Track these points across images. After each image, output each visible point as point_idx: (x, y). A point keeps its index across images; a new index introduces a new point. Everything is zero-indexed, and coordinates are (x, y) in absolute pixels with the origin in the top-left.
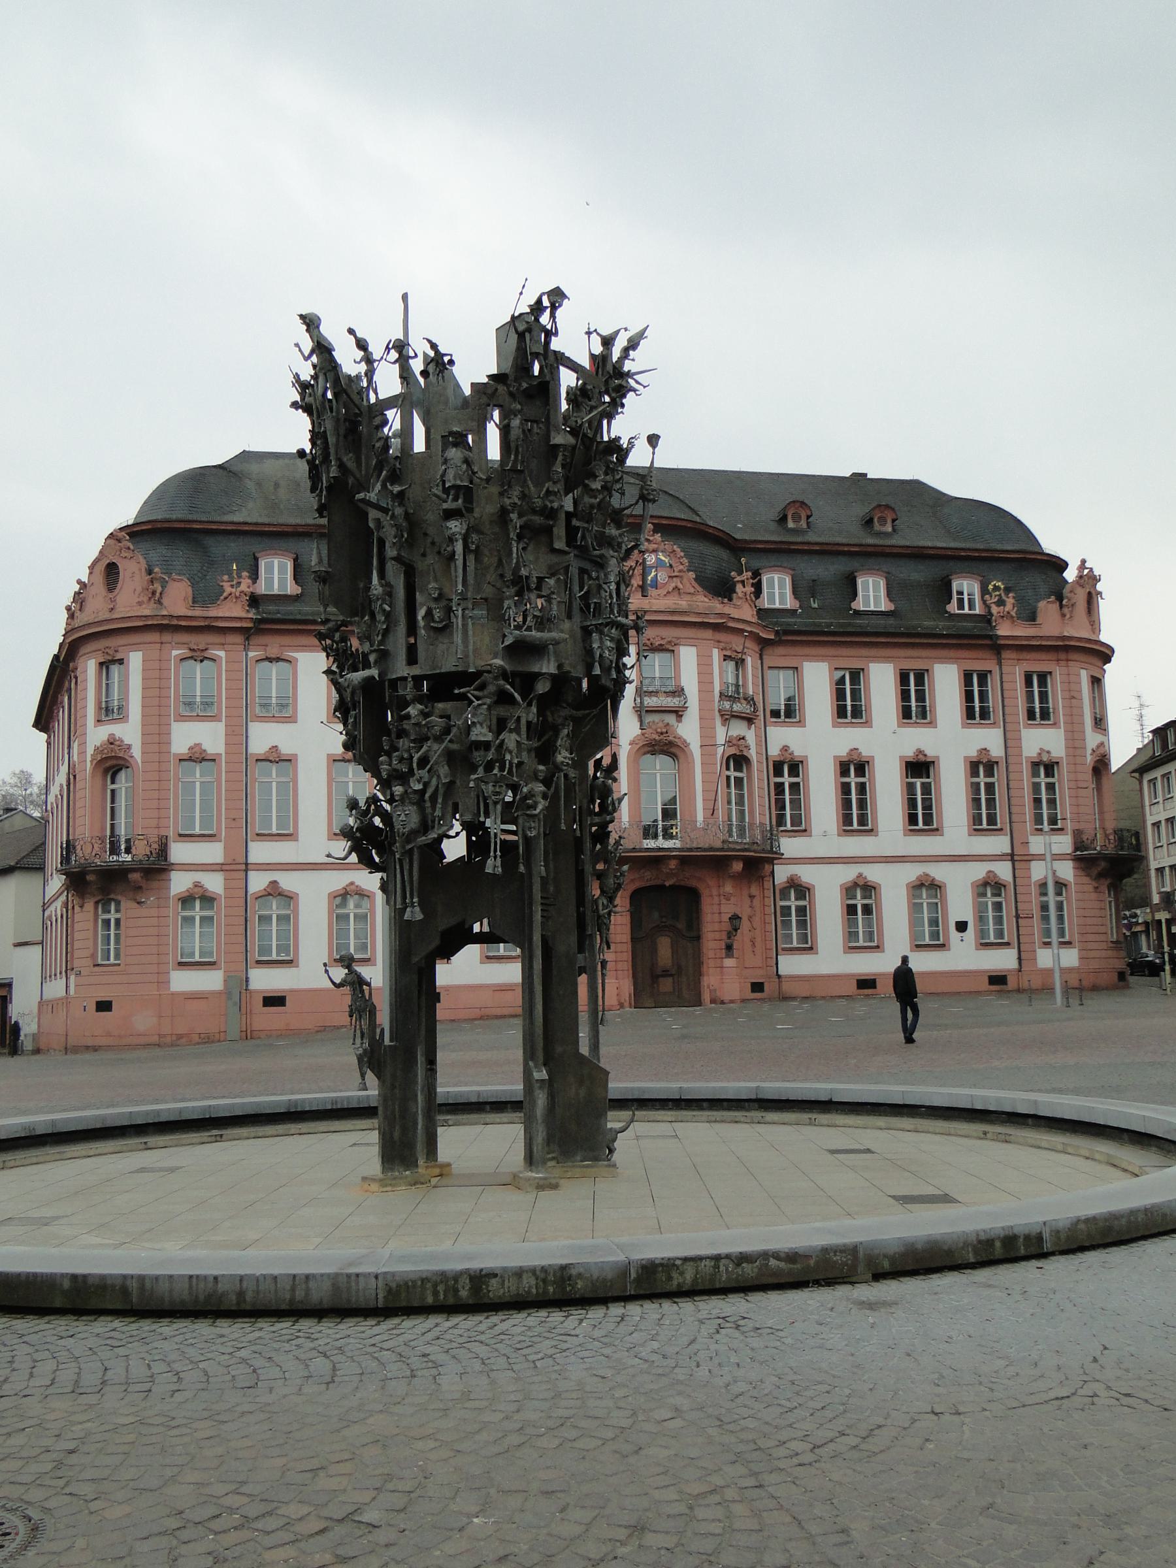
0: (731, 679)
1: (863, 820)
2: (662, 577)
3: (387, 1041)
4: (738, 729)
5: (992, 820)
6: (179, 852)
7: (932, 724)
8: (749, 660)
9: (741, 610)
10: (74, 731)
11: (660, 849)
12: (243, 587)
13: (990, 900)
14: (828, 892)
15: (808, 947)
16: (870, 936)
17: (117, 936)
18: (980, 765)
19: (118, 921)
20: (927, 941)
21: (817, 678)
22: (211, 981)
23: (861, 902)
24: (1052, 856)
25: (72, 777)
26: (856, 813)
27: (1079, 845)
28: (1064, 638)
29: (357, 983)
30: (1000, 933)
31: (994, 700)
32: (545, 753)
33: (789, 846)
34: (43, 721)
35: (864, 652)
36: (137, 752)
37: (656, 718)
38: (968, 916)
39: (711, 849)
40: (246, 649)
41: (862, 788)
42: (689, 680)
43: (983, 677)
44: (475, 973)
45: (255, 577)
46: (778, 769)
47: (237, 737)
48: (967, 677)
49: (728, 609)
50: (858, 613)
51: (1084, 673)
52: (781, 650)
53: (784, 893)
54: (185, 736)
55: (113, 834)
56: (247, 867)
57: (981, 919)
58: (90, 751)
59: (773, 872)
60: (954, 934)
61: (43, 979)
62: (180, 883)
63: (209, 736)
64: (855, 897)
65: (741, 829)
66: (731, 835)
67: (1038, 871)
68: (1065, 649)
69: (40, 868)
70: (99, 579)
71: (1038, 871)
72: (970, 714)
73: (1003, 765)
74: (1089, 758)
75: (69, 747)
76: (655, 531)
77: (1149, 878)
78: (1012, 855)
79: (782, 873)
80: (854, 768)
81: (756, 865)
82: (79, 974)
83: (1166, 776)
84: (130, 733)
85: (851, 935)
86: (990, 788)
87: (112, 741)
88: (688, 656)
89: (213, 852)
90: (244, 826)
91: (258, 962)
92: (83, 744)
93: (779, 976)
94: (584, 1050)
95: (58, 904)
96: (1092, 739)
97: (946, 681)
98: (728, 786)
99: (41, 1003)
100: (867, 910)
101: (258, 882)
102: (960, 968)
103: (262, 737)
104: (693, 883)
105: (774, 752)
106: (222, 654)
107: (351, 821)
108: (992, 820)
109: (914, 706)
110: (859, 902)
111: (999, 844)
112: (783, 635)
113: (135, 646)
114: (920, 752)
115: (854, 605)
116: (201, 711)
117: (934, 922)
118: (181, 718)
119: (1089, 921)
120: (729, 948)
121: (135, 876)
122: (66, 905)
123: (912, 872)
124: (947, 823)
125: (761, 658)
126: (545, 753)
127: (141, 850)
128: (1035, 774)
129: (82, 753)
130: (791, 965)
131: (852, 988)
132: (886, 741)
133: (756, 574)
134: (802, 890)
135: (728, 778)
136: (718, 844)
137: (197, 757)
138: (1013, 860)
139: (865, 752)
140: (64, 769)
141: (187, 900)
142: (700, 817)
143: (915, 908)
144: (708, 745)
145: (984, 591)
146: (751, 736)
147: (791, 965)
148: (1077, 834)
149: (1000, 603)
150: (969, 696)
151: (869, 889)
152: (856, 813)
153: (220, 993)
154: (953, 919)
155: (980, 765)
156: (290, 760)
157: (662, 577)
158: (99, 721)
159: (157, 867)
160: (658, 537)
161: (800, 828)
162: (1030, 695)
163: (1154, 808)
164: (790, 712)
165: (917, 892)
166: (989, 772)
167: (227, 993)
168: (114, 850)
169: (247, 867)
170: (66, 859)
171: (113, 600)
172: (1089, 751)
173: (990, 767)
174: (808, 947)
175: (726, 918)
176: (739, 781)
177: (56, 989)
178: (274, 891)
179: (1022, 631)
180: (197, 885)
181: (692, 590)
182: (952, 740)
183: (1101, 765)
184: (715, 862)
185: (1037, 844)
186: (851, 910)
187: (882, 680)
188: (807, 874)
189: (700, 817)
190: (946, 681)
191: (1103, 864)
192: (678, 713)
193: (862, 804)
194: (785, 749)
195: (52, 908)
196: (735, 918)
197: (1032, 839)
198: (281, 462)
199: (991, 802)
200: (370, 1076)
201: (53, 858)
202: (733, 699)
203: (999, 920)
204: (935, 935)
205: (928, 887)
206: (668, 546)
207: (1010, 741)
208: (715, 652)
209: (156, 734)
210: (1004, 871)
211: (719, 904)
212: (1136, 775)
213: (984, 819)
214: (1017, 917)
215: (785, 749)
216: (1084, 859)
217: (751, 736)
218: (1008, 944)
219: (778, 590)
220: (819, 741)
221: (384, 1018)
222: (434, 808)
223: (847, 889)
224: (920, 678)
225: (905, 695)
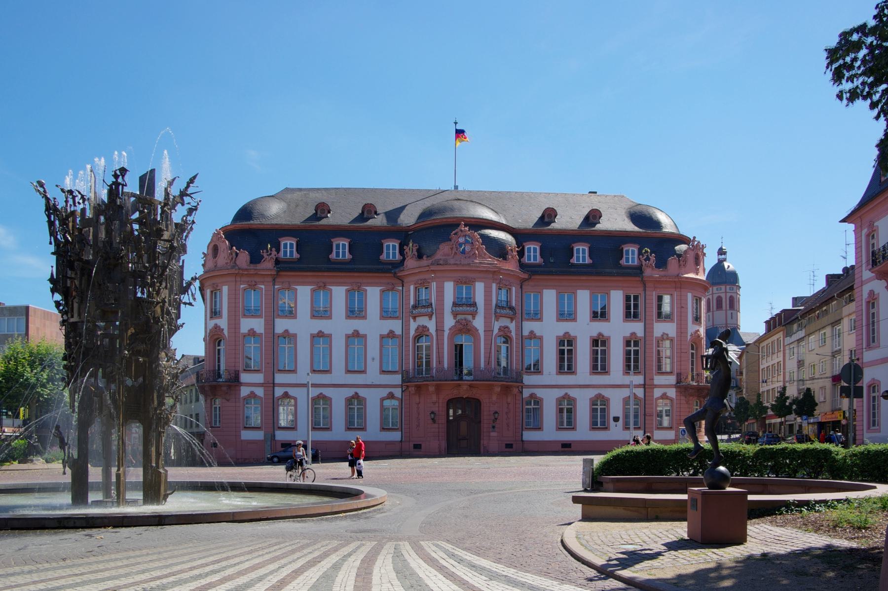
0: (504, 298)
1: (569, 368)
4: (505, 322)
5: (636, 367)
6: (245, 377)
7: (608, 320)
12: (273, 255)
14: (549, 400)
15: (539, 428)
22: (259, 435)
36: (226, 332)
37: (462, 317)
38: (620, 414)
40: (274, 285)
42: (479, 297)
45: (278, 251)
47: (270, 325)
50: (573, 265)
54: (247, 324)
56: (644, 386)
57: (626, 416)
60: (612, 423)
62: (244, 391)
63: (257, 324)
67: (657, 393)
70: (211, 252)
71: (657, 393)
74: (689, 337)
76: (466, 225)
78: (644, 385)
79: (526, 393)
80: (599, 342)
84: (223, 323)
86: (636, 352)
87: (216, 327)
89: (259, 378)
90: (272, 367)
93: (522, 441)
101: (279, 392)
103: (281, 325)
106: (263, 287)
108: (636, 367)
110: (565, 406)
111: (639, 379)
113: (224, 283)
115: (571, 261)
116: (254, 314)
118: (245, 316)
124: (579, 370)
125: (521, 287)
131: (559, 448)
132: (584, 330)
134: (538, 402)
137: (252, 333)
138: (644, 388)
144: (488, 330)
145: (640, 253)
149: (648, 259)
151: (327, 400)
154: (612, 415)
156: (330, 336)
158: (211, 317)
159: (235, 381)
160: (467, 229)
164: (291, 314)
166: (636, 344)
169: (274, 385)
171: (216, 262)
172: (689, 334)
178: (532, 396)
180: (566, 394)
182: (618, 329)
185: (658, 380)
188: (540, 393)
190: (617, 300)
192: (474, 314)
193: (570, 360)
197: (656, 377)
198: (303, 193)
200: (68, 471)
202: (503, 308)
204: (603, 423)
207: (648, 329)
209: (234, 325)
214: (645, 415)
217: (512, 326)
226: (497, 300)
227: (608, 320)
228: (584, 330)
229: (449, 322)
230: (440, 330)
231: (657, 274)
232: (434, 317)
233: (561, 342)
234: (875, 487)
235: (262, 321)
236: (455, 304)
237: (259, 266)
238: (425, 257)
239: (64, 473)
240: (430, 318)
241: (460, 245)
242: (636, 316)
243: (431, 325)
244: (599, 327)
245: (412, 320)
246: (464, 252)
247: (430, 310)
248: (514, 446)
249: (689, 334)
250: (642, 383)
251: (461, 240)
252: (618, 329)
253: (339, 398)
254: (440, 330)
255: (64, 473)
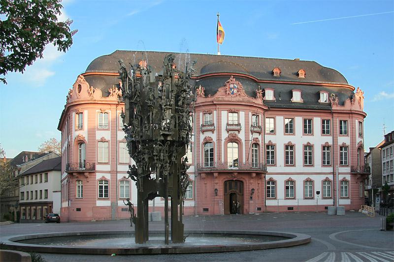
1: (292, 162)
2: (235, 91)
3: (137, 217)
4: (256, 135)
5: (328, 163)
7: (313, 135)
8: (260, 115)
9: (259, 101)
10: (69, 132)
11: (232, 170)
13: (327, 186)
14: (281, 182)
16: (292, 195)
17: (82, 190)
18: (325, 147)
19: (82, 186)
20: (308, 197)
21: (281, 121)
23: (290, 186)
24: (344, 172)
25: (69, 146)
26: (289, 160)
27: (352, 170)
28: (351, 111)
29: (130, 204)
30: (346, 195)
31: (331, 129)
32: (170, 157)
33: (270, 169)
34: (60, 128)
35: (293, 113)
36: (86, 139)
37: (232, 132)
39: (247, 170)
41: (292, 153)
43: (328, 121)
44: (158, 203)
46: (268, 147)
48: (323, 122)
49: (254, 100)
51: (357, 121)
52: (269, 112)
53: (268, 183)
55: (80, 162)
56: (117, 172)
58: (74, 138)
59: (265, 177)
61: (62, 202)
62: (99, 176)
64: (288, 184)
65: (256, 165)
66: (253, 166)
67: (341, 177)
68: (351, 113)
69: (60, 170)
72: (323, 132)
73: (332, 147)
75: (68, 136)
77: (382, 179)
78: (333, 173)
79: (268, 177)
80: (290, 147)
81: (260, 174)
82: (71, 201)
83: (391, 148)
85: (287, 195)
86: (328, 154)
88: (242, 114)
89: (108, 168)
91: (120, 199)
92: (71, 136)
94: (179, 220)
95: (66, 181)
96: (358, 140)
97: (317, 122)
98: (253, 152)
99: (61, 208)
100: (292, 187)
102: (273, 205)
104: (241, 180)
105: (267, 142)
107: (130, 170)
108: (328, 163)
109: (308, 129)
110: (289, 185)
111: (330, 170)
112: (271, 108)
114: (309, 143)
117: (311, 192)
119: (354, 189)
120: (251, 198)
121: (86, 174)
122: (68, 181)
123: (305, 177)
126: (170, 157)
127: (88, 166)
128: (341, 150)
129: (71, 139)
130: (270, 203)
131: (286, 210)
132: (299, 139)
133: (264, 90)
135: (253, 149)
136: (249, 169)
137: (103, 141)
138: (333, 174)
139: (293, 143)
140: (67, 142)
141: (101, 181)
142: (244, 161)
143: (305, 187)
144: (247, 140)
146: (260, 137)
147: (270, 203)
148: (352, 167)
149: (334, 100)
150: (323, 127)
151: (293, 182)
152: (289, 160)
153: (110, 206)
155: (325, 147)
157: (235, 91)
159: (92, 170)
160: (234, 79)
161: (273, 163)
162: (345, 127)
163: (384, 159)
165: (306, 183)
167: (112, 206)
168: (81, 166)
169: (117, 172)
170: (67, 169)
173: (328, 147)
174: (274, 197)
175: (250, 189)
176: (256, 150)
177: (65, 204)
179: (339, 108)
180: (103, 177)
181: (244, 95)
182: (318, 140)
183: (361, 148)
184: (249, 174)
186: (287, 188)
187: (299, 121)
188: (275, 177)
189: (244, 161)
190: (317, 122)
191: (359, 176)
192: (239, 131)
193: (273, 157)
194: (270, 141)
195: (64, 181)
196: (253, 189)
199: (346, 158)
200: (134, 225)
201: (64, 167)
202: (254, 127)
203: (329, 191)
205: (309, 181)
206: (237, 82)
208: (250, 113)
210: (331, 177)
211: (250, 184)
212: (380, 149)
213: (326, 162)
215: (270, 141)
216: (353, 173)
217: (260, 137)
218: (331, 198)
219: (270, 95)
220: (280, 140)
221: (136, 212)
222: (146, 169)
223: (286, 182)
224: (310, 121)
225: (305, 126)
226: (203, 121)
227: (313, 135)
228: (299, 139)
229: (225, 135)
230: (219, 140)
231: (339, 108)
232: (215, 132)
233: (287, 147)
234: (11, 240)
235: (109, 132)
236: (228, 124)
237: (108, 99)
238: (209, 96)
239: (131, 226)
240: (213, 132)
241: (231, 89)
242: (328, 132)
243: (214, 136)
244: (308, 139)
245: (201, 134)
246: (233, 93)
247: (213, 127)
248: (209, 209)
249: (74, 138)
250: (332, 172)
251: (232, 86)
252: (318, 140)
253: (299, 181)
254: (219, 140)
255: (131, 226)
